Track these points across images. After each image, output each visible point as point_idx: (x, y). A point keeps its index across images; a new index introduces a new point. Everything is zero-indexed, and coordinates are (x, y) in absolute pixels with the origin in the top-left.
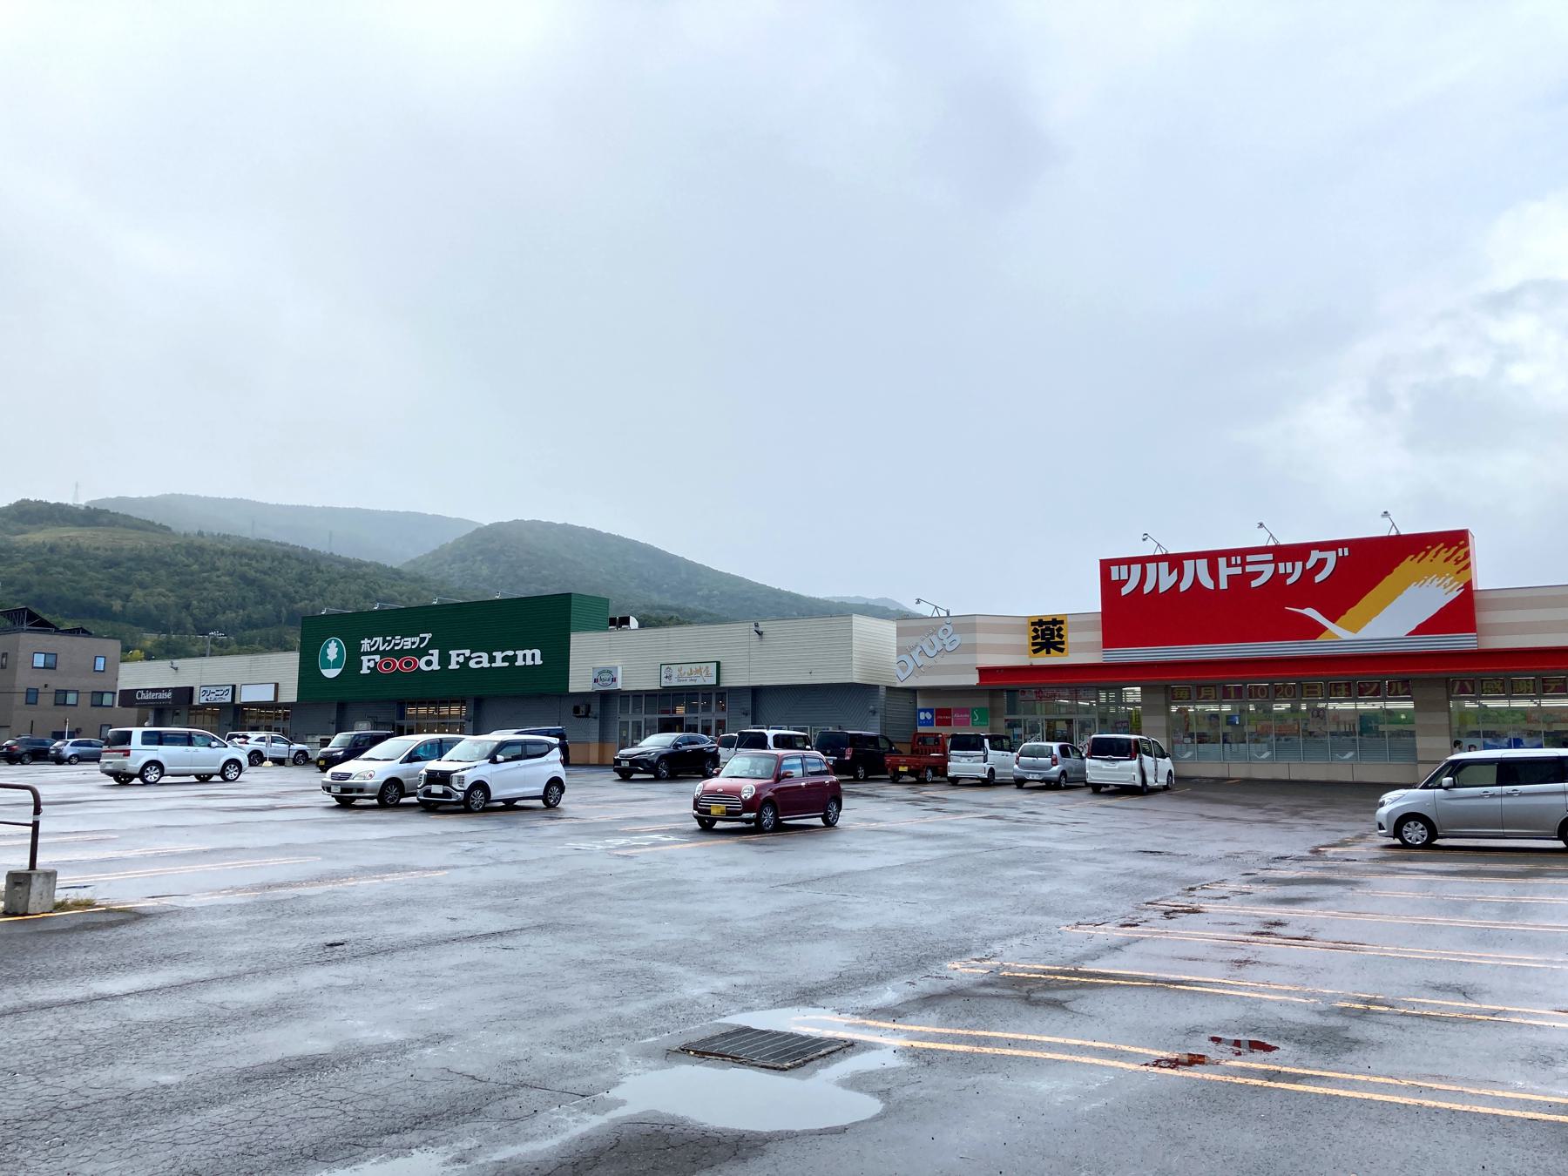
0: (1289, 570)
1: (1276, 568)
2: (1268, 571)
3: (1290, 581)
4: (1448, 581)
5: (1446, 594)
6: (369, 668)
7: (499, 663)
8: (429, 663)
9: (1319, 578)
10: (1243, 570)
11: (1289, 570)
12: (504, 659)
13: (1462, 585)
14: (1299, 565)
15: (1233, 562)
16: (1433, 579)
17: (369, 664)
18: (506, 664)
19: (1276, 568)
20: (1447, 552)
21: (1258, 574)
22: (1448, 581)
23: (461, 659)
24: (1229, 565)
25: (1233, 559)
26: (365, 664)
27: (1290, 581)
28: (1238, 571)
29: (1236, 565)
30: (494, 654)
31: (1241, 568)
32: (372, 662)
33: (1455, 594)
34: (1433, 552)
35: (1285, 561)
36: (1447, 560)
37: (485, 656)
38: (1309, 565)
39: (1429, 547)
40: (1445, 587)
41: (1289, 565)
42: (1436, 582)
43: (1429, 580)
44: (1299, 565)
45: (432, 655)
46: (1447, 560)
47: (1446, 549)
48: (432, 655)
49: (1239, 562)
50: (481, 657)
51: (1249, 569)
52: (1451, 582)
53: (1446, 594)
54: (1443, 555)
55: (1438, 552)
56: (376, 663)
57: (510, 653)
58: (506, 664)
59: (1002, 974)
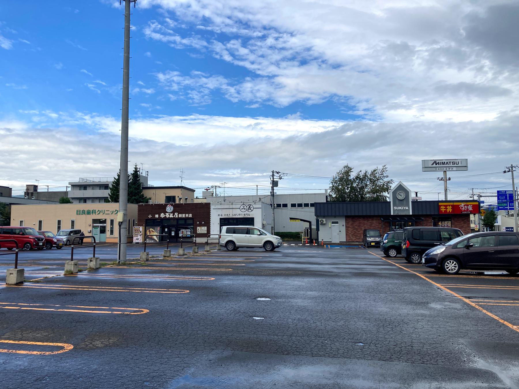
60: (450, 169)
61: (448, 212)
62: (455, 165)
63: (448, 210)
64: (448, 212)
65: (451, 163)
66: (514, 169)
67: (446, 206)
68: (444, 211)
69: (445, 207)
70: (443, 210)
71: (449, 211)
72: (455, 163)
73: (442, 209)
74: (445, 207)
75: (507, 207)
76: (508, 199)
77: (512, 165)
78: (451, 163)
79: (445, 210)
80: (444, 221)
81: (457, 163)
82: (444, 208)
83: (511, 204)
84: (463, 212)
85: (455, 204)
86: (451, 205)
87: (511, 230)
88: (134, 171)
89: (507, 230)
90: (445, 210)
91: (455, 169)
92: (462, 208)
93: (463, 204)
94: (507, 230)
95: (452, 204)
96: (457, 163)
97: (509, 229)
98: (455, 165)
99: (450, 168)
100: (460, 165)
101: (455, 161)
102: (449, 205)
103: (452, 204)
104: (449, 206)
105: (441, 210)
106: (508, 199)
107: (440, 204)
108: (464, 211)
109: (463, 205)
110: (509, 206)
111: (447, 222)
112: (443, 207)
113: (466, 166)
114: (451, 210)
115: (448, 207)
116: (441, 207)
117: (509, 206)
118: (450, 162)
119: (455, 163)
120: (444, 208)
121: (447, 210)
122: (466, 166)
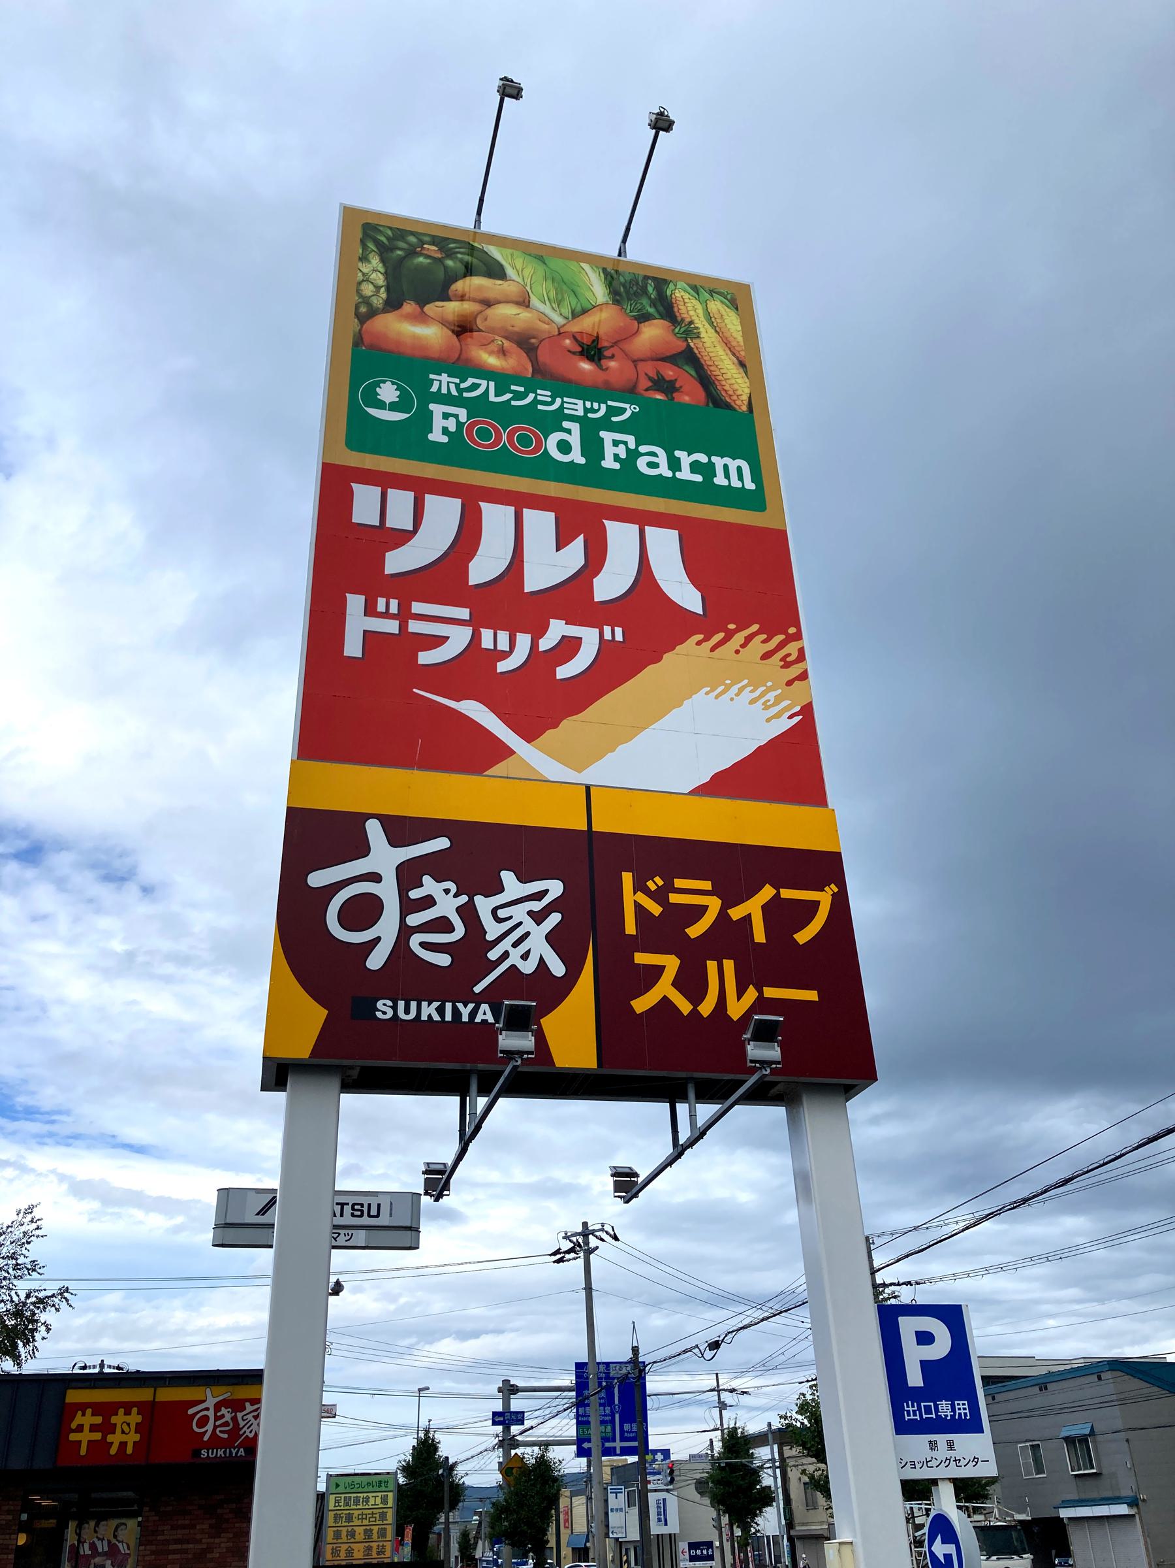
0: (503, 644)
1: (476, 638)
2: (458, 639)
3: (503, 666)
4: (771, 696)
5: (768, 720)
6: (445, 431)
7: (685, 474)
8: (564, 447)
9: (564, 672)
10: (403, 626)
11: (503, 644)
12: (695, 467)
13: (798, 709)
14: (524, 641)
15: (381, 607)
16: (744, 687)
17: (445, 423)
18: (699, 478)
19: (476, 638)
20: (764, 642)
21: (440, 640)
22: (771, 696)
23: (622, 451)
24: (370, 610)
25: (381, 602)
26: (438, 423)
27: (503, 666)
28: (392, 627)
29: (387, 615)
30: (677, 453)
31: (397, 622)
32: (452, 420)
33: (785, 724)
34: (740, 637)
35: (496, 628)
36: (766, 656)
37: (662, 458)
38: (545, 644)
39: (732, 626)
40: (766, 707)
41: (503, 638)
42: (747, 695)
43: (735, 689)
44: (524, 641)
45: (569, 431)
46: (766, 656)
47: (764, 636)
48: (569, 431)
49: (394, 609)
50: (654, 454)
51: (414, 627)
52: (777, 703)
53: (768, 720)
54: (758, 646)
55: (749, 639)
56: (459, 425)
57: (702, 458)
58: (699, 478)
59: (19, 1342)
60: (341, 1241)
61: (113, 1451)
62: (365, 1220)
63: (115, 1439)
64: (113, 1451)
65: (348, 1209)
66: (593, 1242)
67: (106, 1410)
68: (91, 1443)
69: (98, 1420)
70: (85, 1438)
71: (123, 1445)
72: (365, 1209)
73: (80, 1428)
74: (98, 1420)
75: (614, 1440)
76: (617, 1402)
77: (585, 1224)
78: (348, 1209)
79: (97, 1436)
80: (101, 1518)
81: (374, 1212)
82: (93, 1428)
83: (627, 1427)
84: (204, 1453)
85: (168, 1394)
86: (142, 1406)
87: (705, 1552)
88: (447, 1458)
89: (693, 1552)
90: (97, 1436)
91: (360, 1237)
92: (204, 1421)
93: (211, 1397)
94: (693, 1552)
95: (144, 1394)
96: (374, 1212)
97: (699, 1552)
98: (365, 1220)
99: (342, 1232)
100: (384, 1220)
101: (365, 1200)
102: (128, 1407)
103: (144, 1394)
104: (128, 1413)
105: (73, 1437)
106: (617, 1402)
107: (74, 1396)
108: (215, 1441)
109: (211, 1402)
110: (623, 1439)
111: (114, 1523)
112: (87, 1419)
113: (409, 1228)
114: (133, 1438)
115: (118, 1419)
116: (79, 1419)
117: (623, 1439)
118: (342, 1205)
119: (365, 1209)
120: (93, 1428)
121: (110, 1438)
122: (409, 1228)
